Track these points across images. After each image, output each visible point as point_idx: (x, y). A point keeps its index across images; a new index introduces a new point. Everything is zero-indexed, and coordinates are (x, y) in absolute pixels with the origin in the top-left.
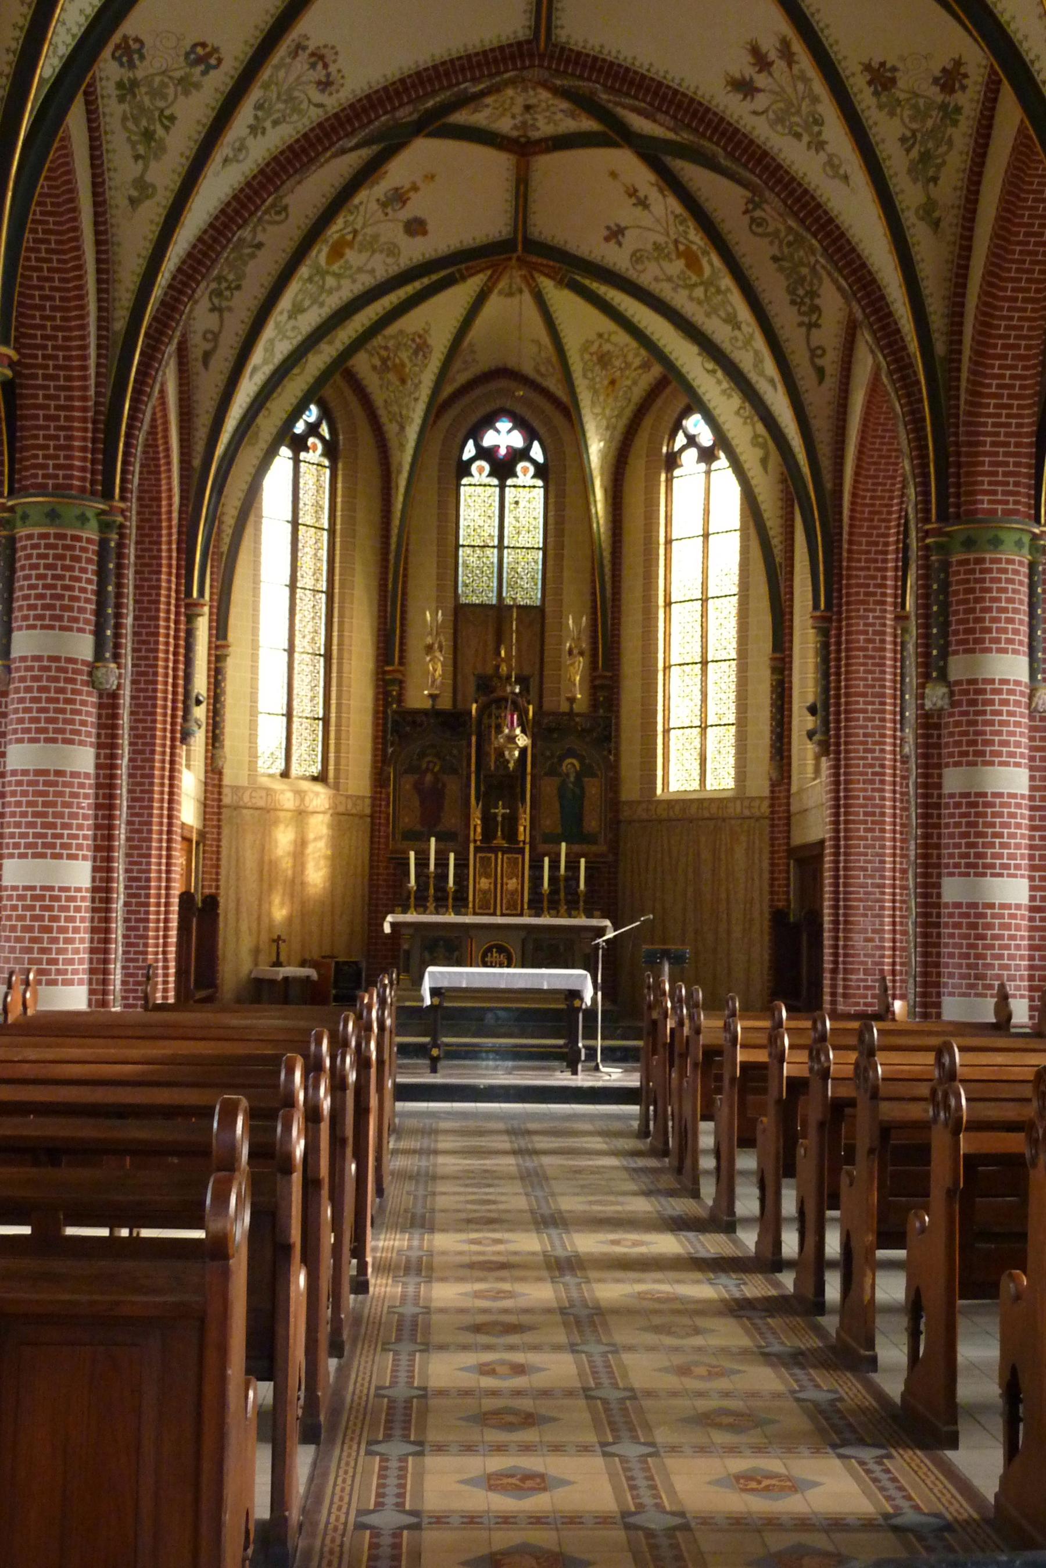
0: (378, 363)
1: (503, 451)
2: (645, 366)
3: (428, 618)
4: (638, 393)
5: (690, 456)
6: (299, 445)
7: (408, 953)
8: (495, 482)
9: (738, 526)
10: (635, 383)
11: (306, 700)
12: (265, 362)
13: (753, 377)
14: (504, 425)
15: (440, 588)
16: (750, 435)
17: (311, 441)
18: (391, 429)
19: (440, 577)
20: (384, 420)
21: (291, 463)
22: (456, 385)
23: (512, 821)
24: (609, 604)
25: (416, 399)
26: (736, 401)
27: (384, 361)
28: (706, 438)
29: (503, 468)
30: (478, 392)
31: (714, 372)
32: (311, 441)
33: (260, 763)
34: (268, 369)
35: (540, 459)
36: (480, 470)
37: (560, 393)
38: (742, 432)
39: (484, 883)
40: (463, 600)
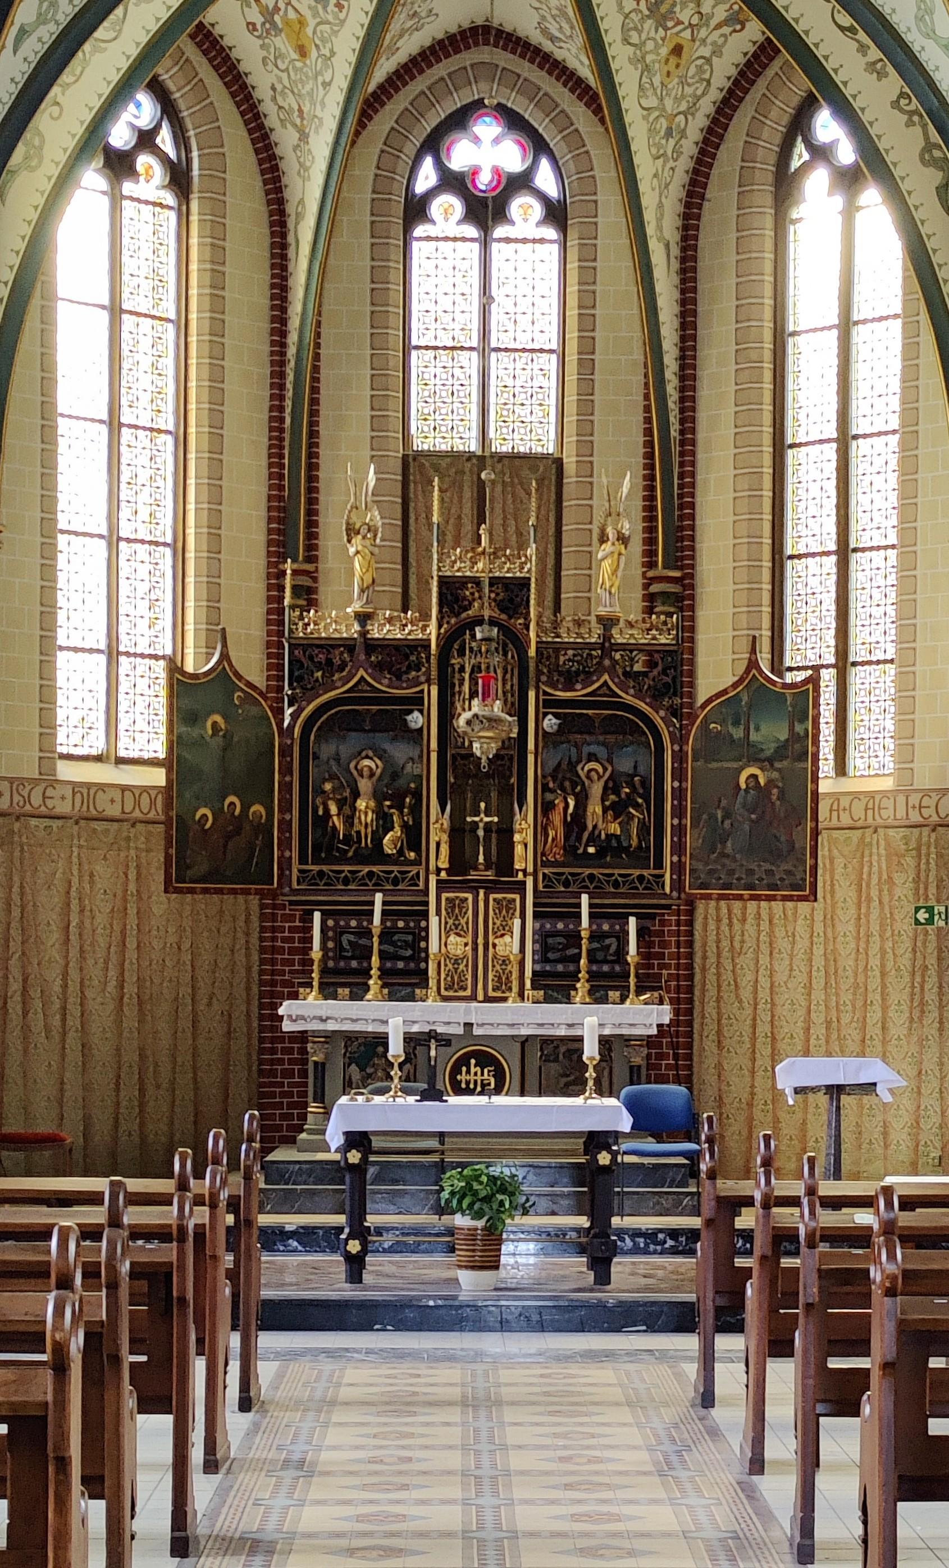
0: (259, 19)
1: (484, 179)
2: (736, 21)
3: (354, 484)
4: (724, 70)
5: (817, 183)
6: (120, 165)
7: (320, 1068)
8: (471, 231)
9: (897, 308)
10: (717, 52)
11: (143, 625)
12: (41, 20)
13: (915, 39)
14: (487, 128)
15: (377, 423)
16: (921, 143)
17: (144, 161)
18: (285, 139)
19: (377, 404)
20: (272, 121)
21: (105, 201)
22: (401, 57)
23: (505, 833)
24: (675, 449)
25: (326, 85)
26: (894, 83)
27: (269, 14)
28: (846, 154)
29: (486, 210)
30: (441, 70)
31: (851, 30)
32: (144, 161)
33: (61, 738)
34: (47, 33)
35: (552, 190)
36: (447, 211)
37: (584, 68)
38: (904, 140)
39: (457, 946)
40: (421, 443)
